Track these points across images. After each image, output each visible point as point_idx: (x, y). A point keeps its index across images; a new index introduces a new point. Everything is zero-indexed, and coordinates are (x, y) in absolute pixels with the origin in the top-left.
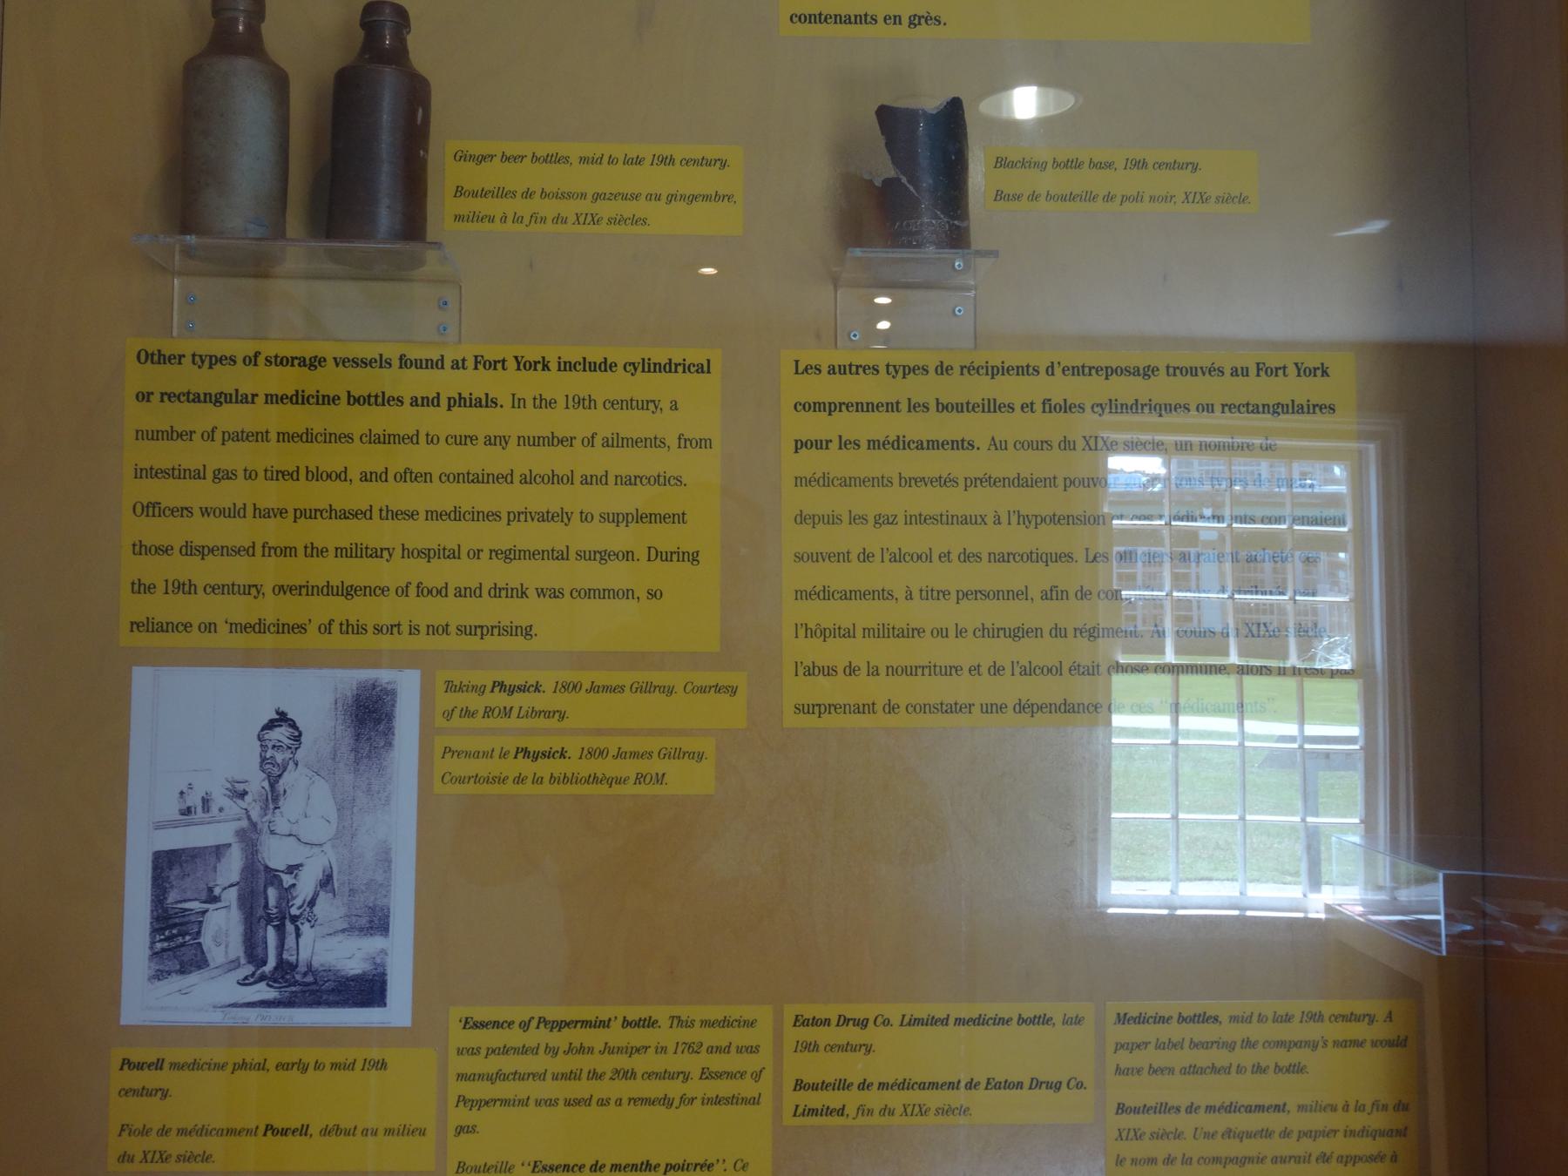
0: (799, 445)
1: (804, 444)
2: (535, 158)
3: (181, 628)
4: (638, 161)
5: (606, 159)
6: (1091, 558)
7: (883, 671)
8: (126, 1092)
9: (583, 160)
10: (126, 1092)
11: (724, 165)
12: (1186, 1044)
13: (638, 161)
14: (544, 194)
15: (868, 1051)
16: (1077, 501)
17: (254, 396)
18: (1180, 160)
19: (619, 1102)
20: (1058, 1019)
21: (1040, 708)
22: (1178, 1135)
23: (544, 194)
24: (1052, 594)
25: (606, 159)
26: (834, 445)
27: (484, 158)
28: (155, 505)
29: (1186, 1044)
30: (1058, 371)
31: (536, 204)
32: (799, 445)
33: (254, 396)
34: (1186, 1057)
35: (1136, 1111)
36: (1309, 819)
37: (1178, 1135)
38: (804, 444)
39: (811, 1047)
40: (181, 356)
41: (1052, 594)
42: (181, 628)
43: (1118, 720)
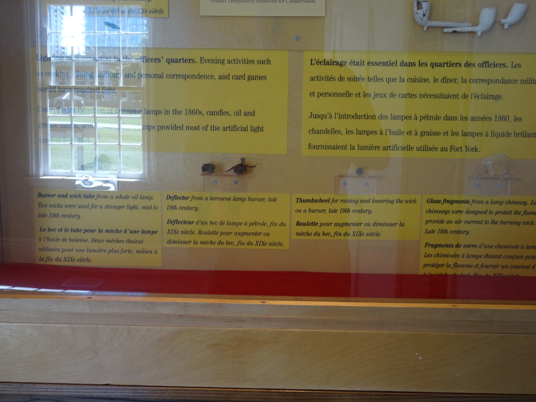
4: (335, 211)
5: (153, 207)
6: (514, 66)
9: (144, 208)
11: (370, 212)
12: (139, 197)
13: (335, 211)
15: (370, 213)
16: (153, 120)
18: (190, 206)
19: (305, 211)
22: (192, 233)
25: (153, 207)
27: (120, 207)
29: (139, 197)
34: (476, 88)
35: (304, 224)
37: (192, 233)
39: (174, 208)
43: (140, 127)
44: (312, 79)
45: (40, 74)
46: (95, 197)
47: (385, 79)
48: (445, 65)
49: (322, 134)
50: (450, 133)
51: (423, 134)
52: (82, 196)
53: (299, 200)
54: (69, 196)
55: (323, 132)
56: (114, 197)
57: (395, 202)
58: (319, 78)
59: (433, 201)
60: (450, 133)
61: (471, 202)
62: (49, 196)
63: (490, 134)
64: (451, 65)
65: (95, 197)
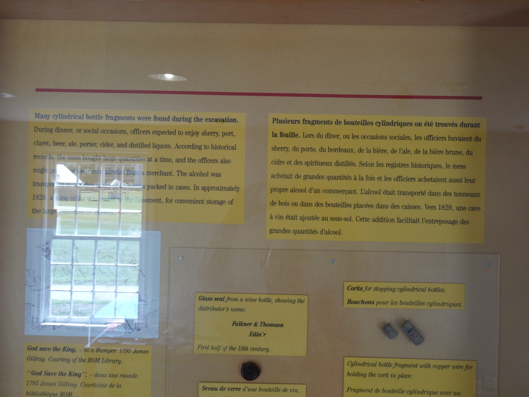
7: (279, 135)
44: (273, 176)
45: (79, 171)
46: (393, 366)
47: (325, 177)
49: (169, 176)
50: (383, 178)
51: (305, 177)
52: (389, 376)
53: (263, 324)
54: (38, 349)
55: (315, 178)
56: (244, 300)
57: (297, 301)
58: (279, 176)
59: (204, 299)
60: (383, 178)
61: (364, 289)
62: (460, 194)
63: (358, 178)
65: (393, 366)
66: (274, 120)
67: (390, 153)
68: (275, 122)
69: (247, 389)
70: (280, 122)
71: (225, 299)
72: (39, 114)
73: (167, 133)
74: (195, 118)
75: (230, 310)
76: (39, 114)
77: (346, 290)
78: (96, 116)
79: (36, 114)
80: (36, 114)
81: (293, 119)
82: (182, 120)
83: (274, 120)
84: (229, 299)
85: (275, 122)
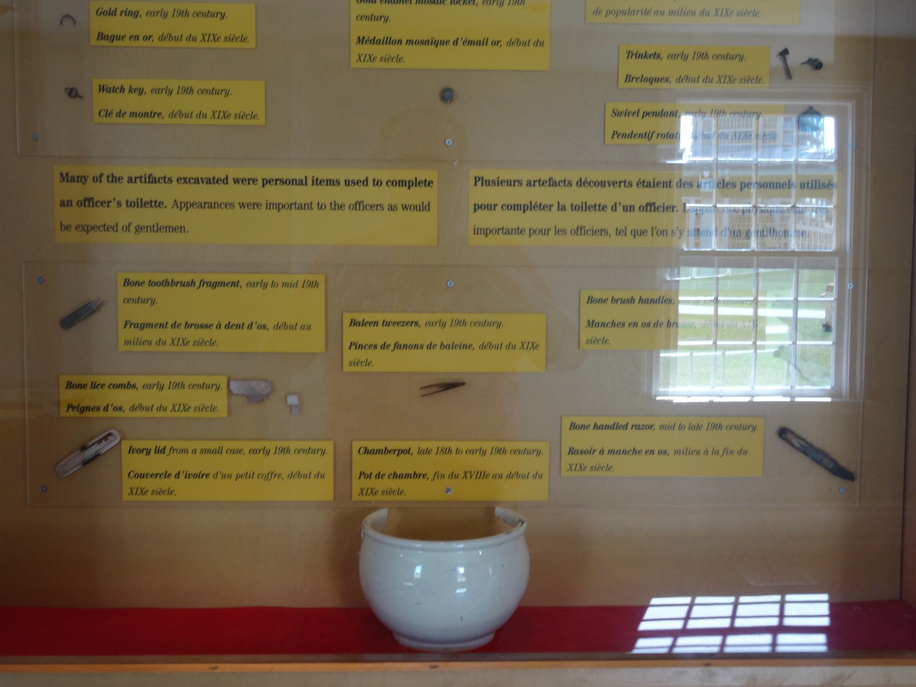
0: (477, 207)
1: (480, 207)
2: (596, 427)
3: (223, 206)
7: (568, 207)
8: (128, 301)
10: (128, 301)
14: (188, 325)
17: (495, 205)
20: (169, 203)
21: (192, 205)
23: (188, 325)
24: (650, 207)
26: (555, 208)
28: (359, 203)
30: (620, 208)
31: (182, 332)
32: (477, 207)
33: (495, 205)
36: (718, 206)
38: (480, 207)
40: (551, 206)
41: (650, 207)
42: (223, 206)
48: (138, 180)
64: (552, 183)
66: (477, 179)
67: (271, 329)
68: (479, 183)
69: (219, 476)
70: (487, 183)
71: (167, 451)
72: (67, 174)
73: (102, 229)
74: (108, 177)
75: (190, 451)
76: (67, 174)
77: (584, 306)
78: (141, 177)
79: (62, 174)
80: (62, 174)
81: (509, 178)
82: (537, 184)
83: (477, 179)
84: (172, 450)
85: (479, 183)
